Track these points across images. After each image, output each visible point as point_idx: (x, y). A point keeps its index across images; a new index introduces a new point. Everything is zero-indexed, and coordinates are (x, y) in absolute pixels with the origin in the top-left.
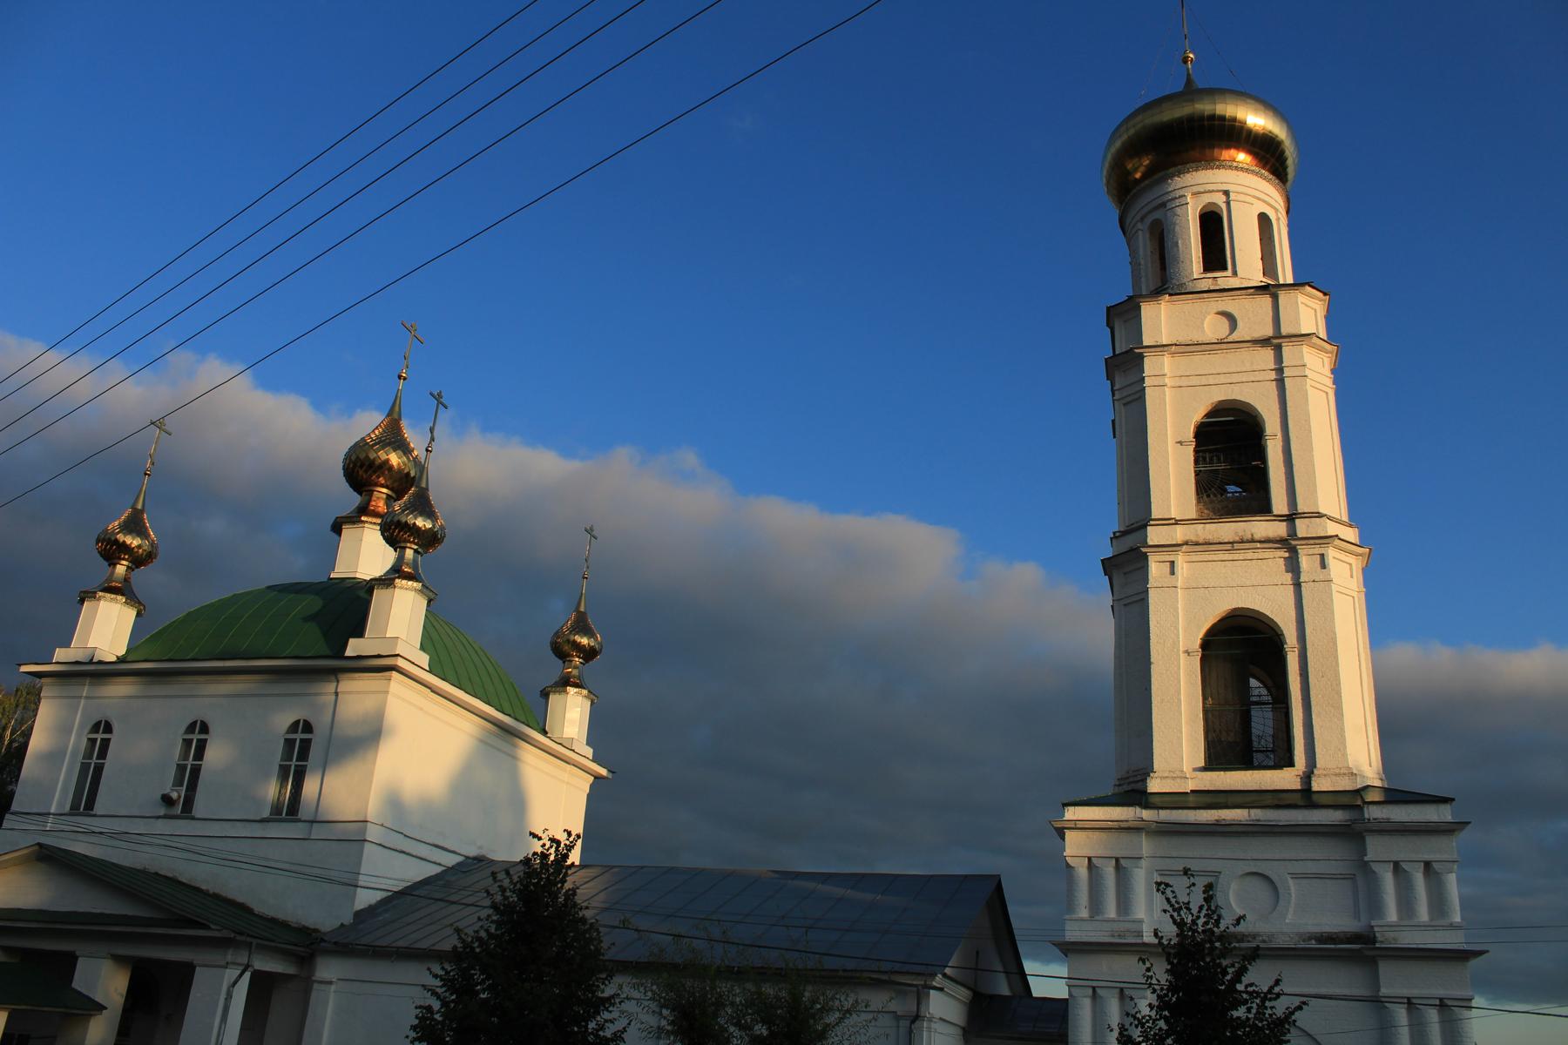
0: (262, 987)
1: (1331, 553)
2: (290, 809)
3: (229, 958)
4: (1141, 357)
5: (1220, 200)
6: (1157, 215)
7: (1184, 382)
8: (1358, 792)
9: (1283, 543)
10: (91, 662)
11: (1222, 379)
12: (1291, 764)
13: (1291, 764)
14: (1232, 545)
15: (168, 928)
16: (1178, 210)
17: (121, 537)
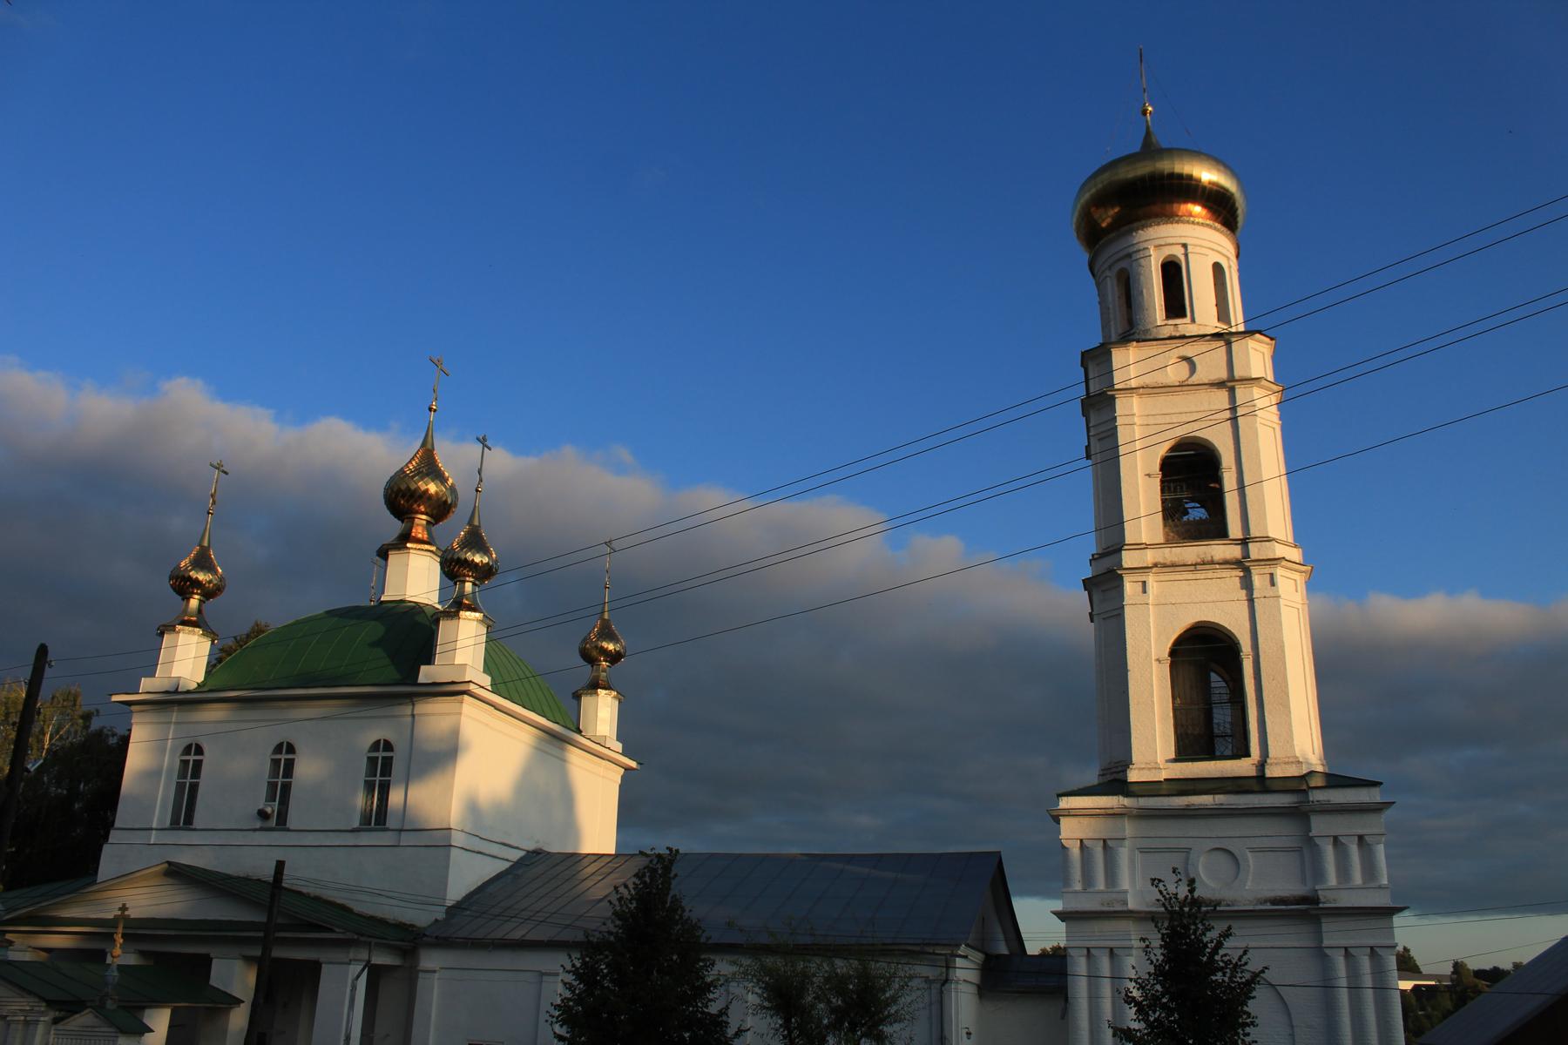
0: (376, 975)
1: (1280, 572)
2: (377, 818)
3: (351, 956)
4: (1113, 398)
5: (1178, 252)
6: (1123, 264)
7: (1151, 420)
8: (1303, 778)
10: (176, 692)
12: (1248, 755)
13: (1248, 755)
14: (1196, 566)
15: (289, 931)
17: (193, 574)
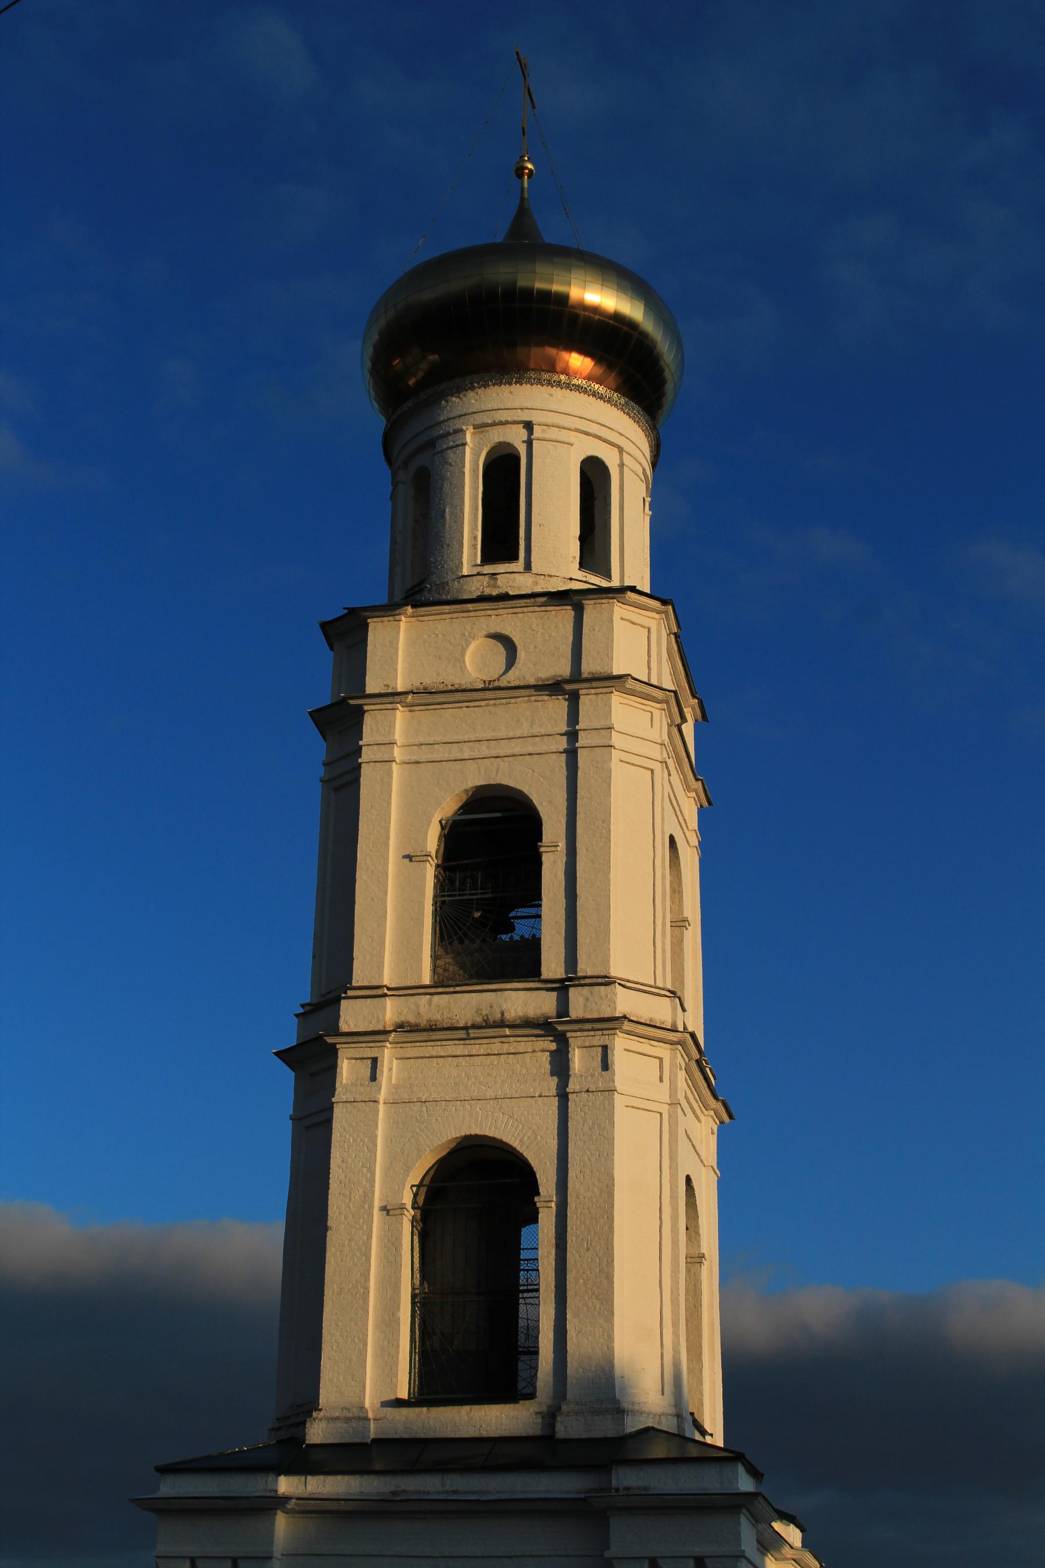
5: (516, 437)
7: (425, 755)
9: (543, 1026)
11: (484, 750)
13: (531, 1396)
14: (467, 1032)
16: (451, 456)
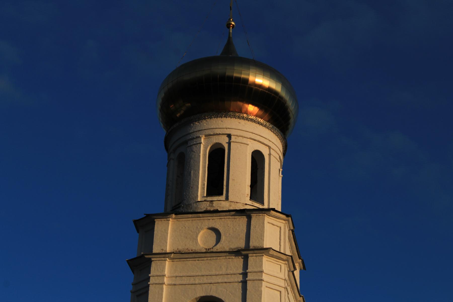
5: (224, 141)
